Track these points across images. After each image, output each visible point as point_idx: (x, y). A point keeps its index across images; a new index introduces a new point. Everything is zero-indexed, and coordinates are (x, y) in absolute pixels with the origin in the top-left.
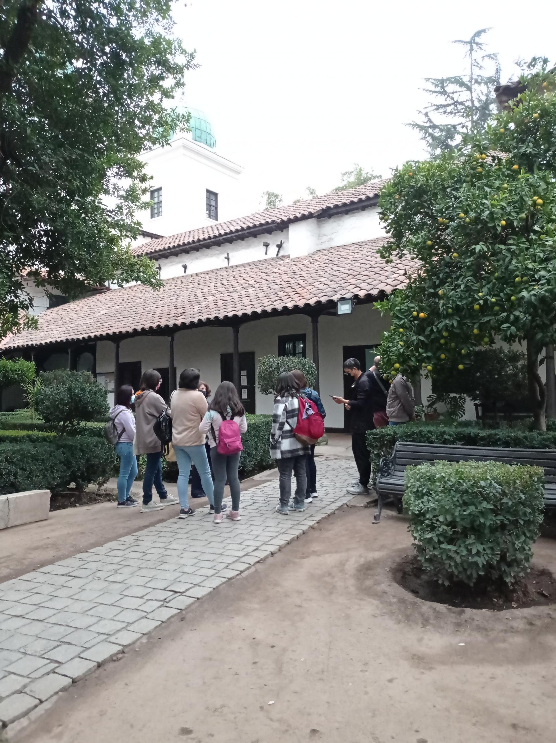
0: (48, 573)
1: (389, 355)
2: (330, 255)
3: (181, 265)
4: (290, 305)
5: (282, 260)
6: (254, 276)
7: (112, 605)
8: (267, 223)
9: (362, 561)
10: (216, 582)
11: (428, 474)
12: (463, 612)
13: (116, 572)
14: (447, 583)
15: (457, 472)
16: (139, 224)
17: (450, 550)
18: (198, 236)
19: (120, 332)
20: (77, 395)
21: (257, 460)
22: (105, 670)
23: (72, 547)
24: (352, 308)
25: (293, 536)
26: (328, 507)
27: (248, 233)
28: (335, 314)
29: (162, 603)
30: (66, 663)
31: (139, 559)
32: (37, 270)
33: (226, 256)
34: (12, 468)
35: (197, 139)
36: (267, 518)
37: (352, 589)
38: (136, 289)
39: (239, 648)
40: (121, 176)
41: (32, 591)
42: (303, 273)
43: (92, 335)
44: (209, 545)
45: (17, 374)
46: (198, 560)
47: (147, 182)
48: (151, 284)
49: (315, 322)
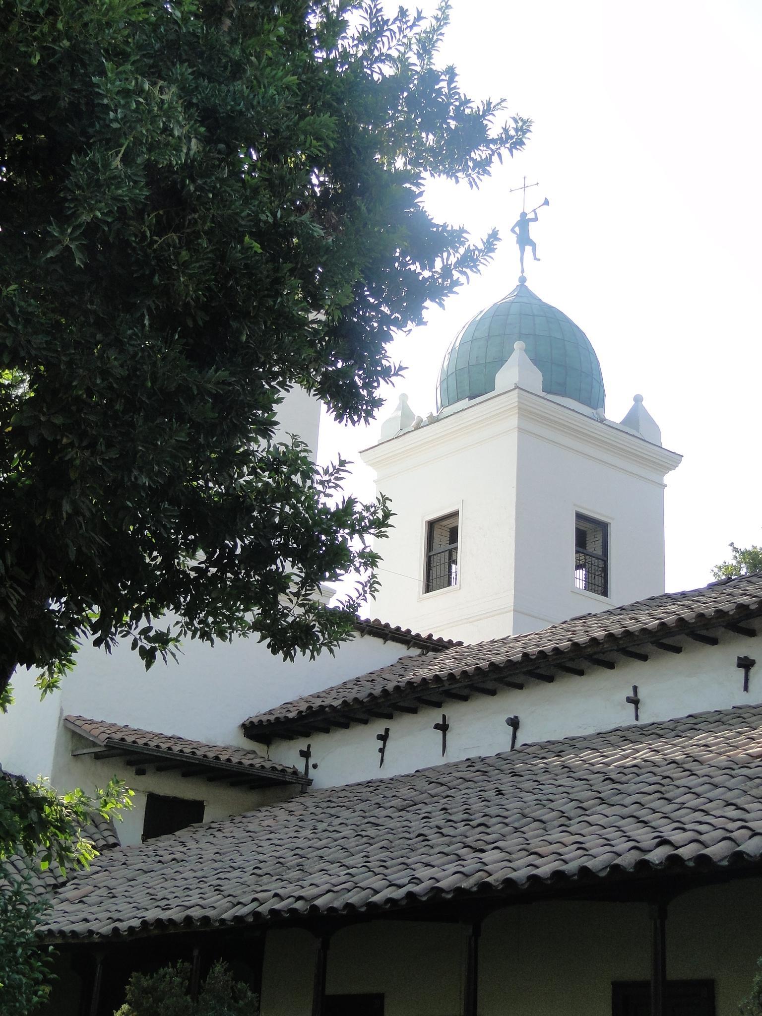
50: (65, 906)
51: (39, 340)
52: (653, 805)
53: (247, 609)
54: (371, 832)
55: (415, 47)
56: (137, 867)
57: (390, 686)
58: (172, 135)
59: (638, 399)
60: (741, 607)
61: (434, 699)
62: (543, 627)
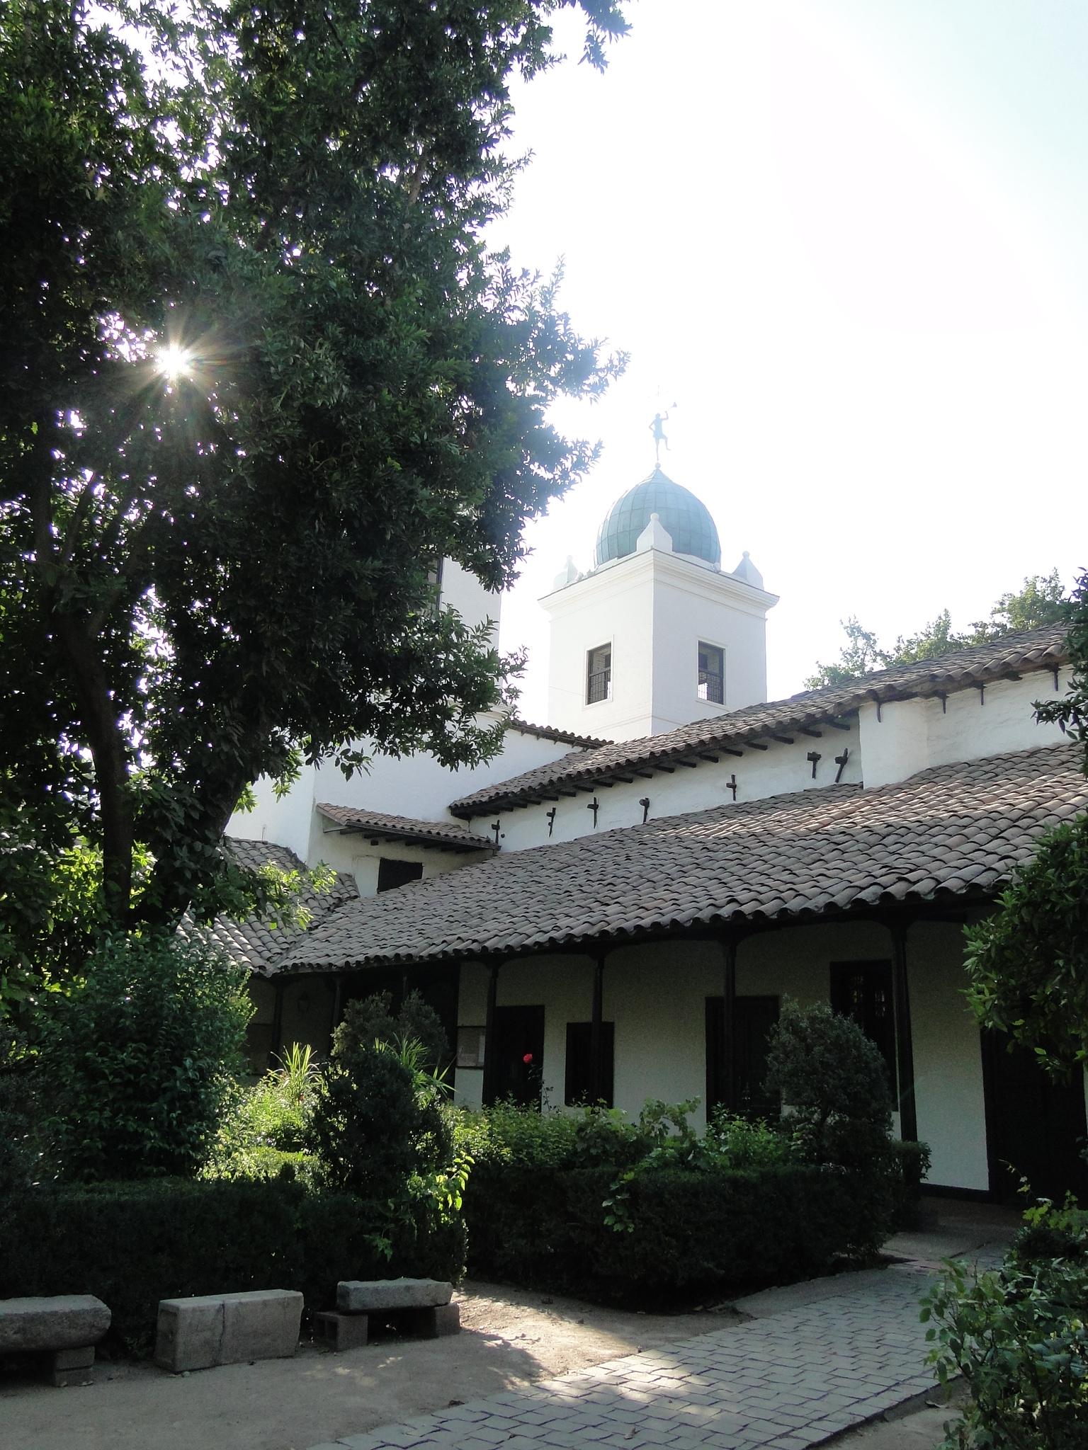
50: (316, 945)
51: (233, 542)
52: (732, 870)
53: (423, 733)
54: (534, 888)
55: (539, 298)
56: (369, 914)
57: (555, 778)
58: (322, 383)
59: (746, 555)
60: (809, 716)
61: (588, 786)
62: (670, 729)
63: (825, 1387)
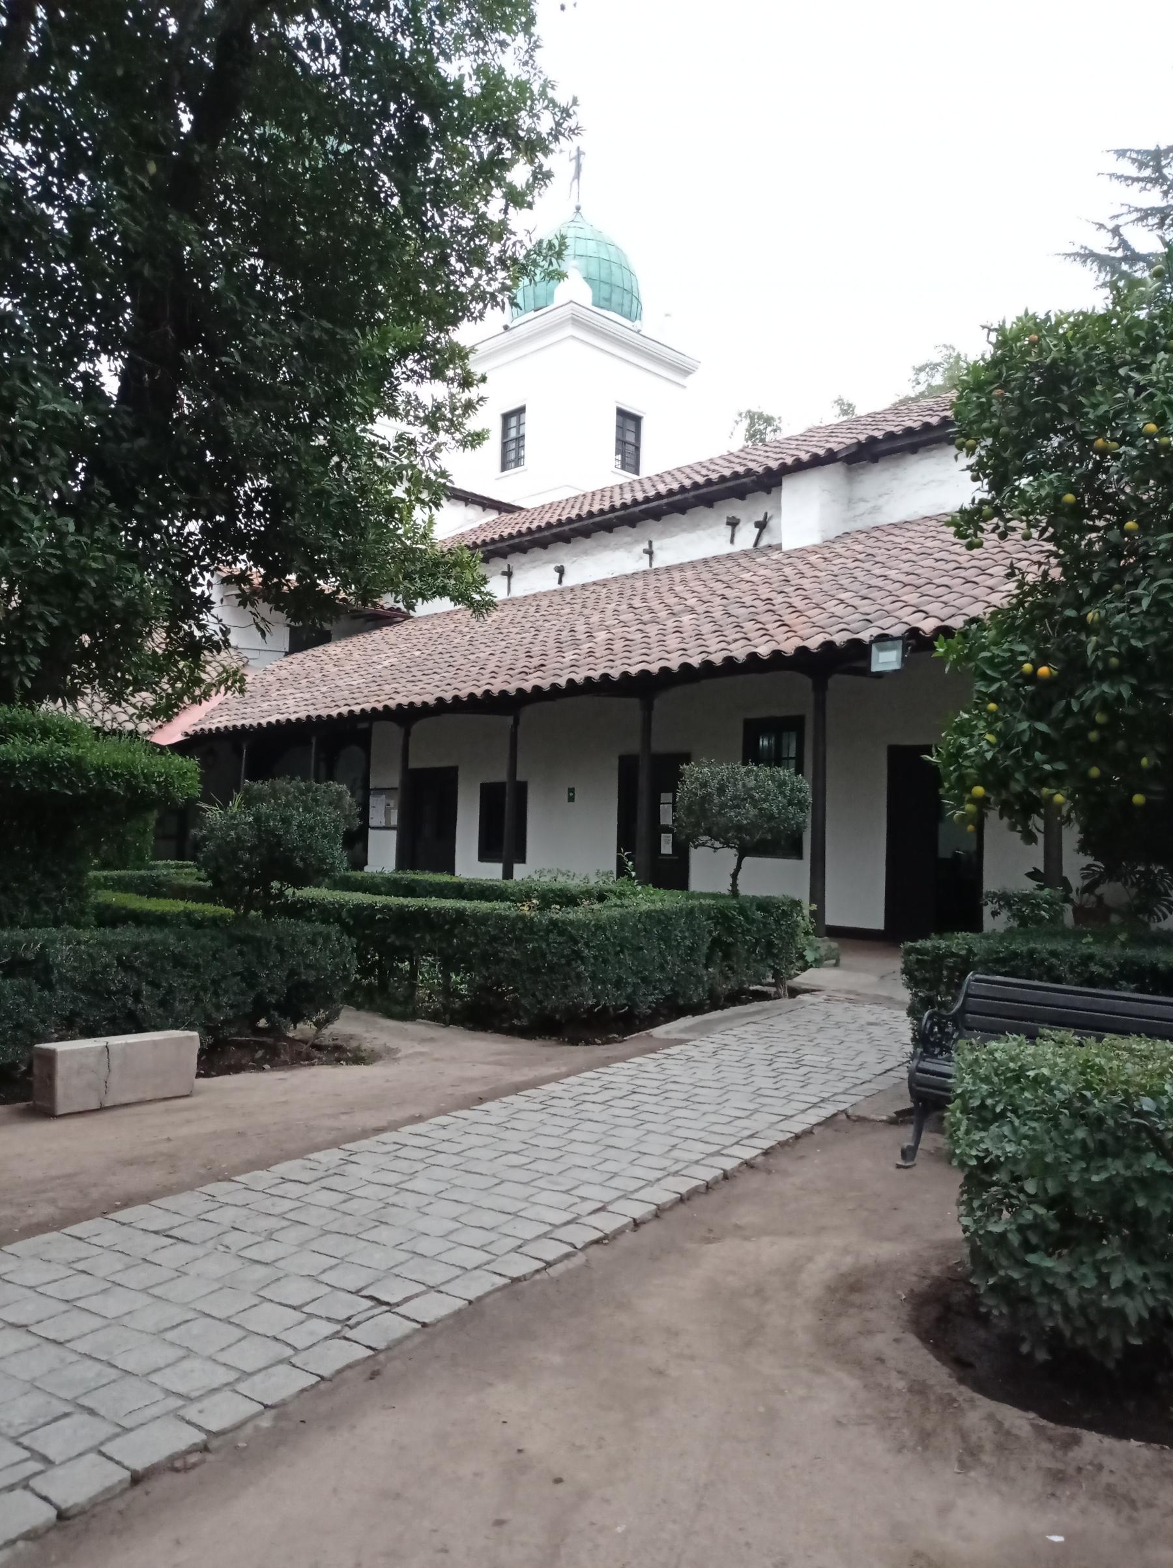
0: (129, 1224)
1: (960, 766)
2: (871, 542)
3: (553, 566)
4: (764, 650)
5: (766, 555)
6: (700, 589)
7: (228, 1321)
8: (736, 475)
9: (848, 1262)
10: (479, 1285)
11: (1012, 1065)
12: (1076, 1441)
13: (270, 1236)
14: (1042, 1356)
15: (1087, 1066)
16: (443, 474)
17: (1050, 1271)
18: (591, 505)
19: (411, 704)
20: (271, 832)
21: (662, 992)
22: (147, 1493)
23: (204, 1166)
24: (903, 659)
25: (695, 1183)
26: (800, 1117)
27: (694, 497)
28: (865, 671)
29: (338, 1327)
30: (63, 1463)
31: (332, 1209)
32: (243, 572)
33: (647, 546)
34: (131, 981)
35: (602, 303)
36: (649, 1132)
37: (802, 1339)
38: (459, 616)
39: (476, 1474)
40: (422, 377)
41: (75, 1266)
42: (806, 583)
43: (357, 709)
44: (498, 1189)
45: (155, 782)
46: (459, 1225)
47: (474, 389)
48: (471, 603)
49: (820, 688)
63: (752, 1106)
